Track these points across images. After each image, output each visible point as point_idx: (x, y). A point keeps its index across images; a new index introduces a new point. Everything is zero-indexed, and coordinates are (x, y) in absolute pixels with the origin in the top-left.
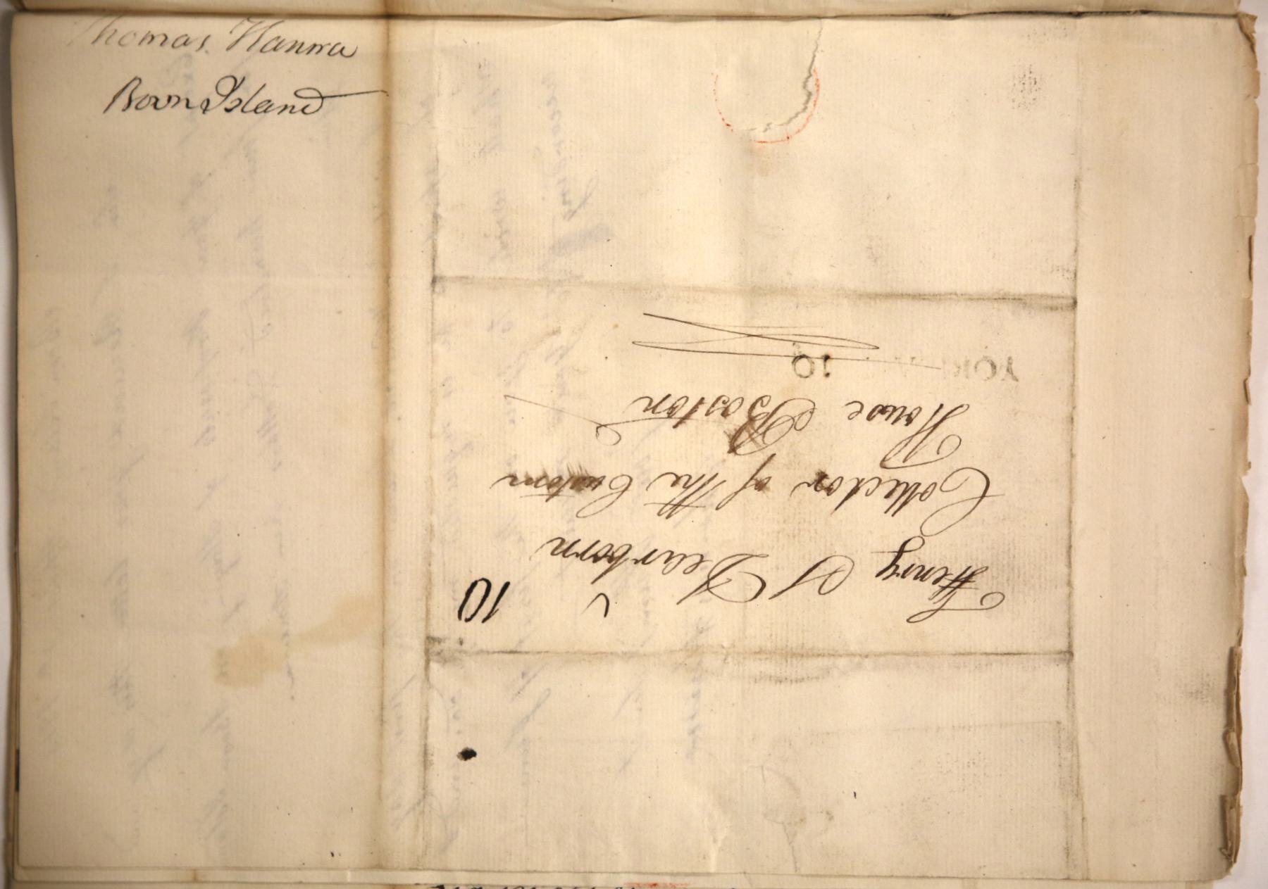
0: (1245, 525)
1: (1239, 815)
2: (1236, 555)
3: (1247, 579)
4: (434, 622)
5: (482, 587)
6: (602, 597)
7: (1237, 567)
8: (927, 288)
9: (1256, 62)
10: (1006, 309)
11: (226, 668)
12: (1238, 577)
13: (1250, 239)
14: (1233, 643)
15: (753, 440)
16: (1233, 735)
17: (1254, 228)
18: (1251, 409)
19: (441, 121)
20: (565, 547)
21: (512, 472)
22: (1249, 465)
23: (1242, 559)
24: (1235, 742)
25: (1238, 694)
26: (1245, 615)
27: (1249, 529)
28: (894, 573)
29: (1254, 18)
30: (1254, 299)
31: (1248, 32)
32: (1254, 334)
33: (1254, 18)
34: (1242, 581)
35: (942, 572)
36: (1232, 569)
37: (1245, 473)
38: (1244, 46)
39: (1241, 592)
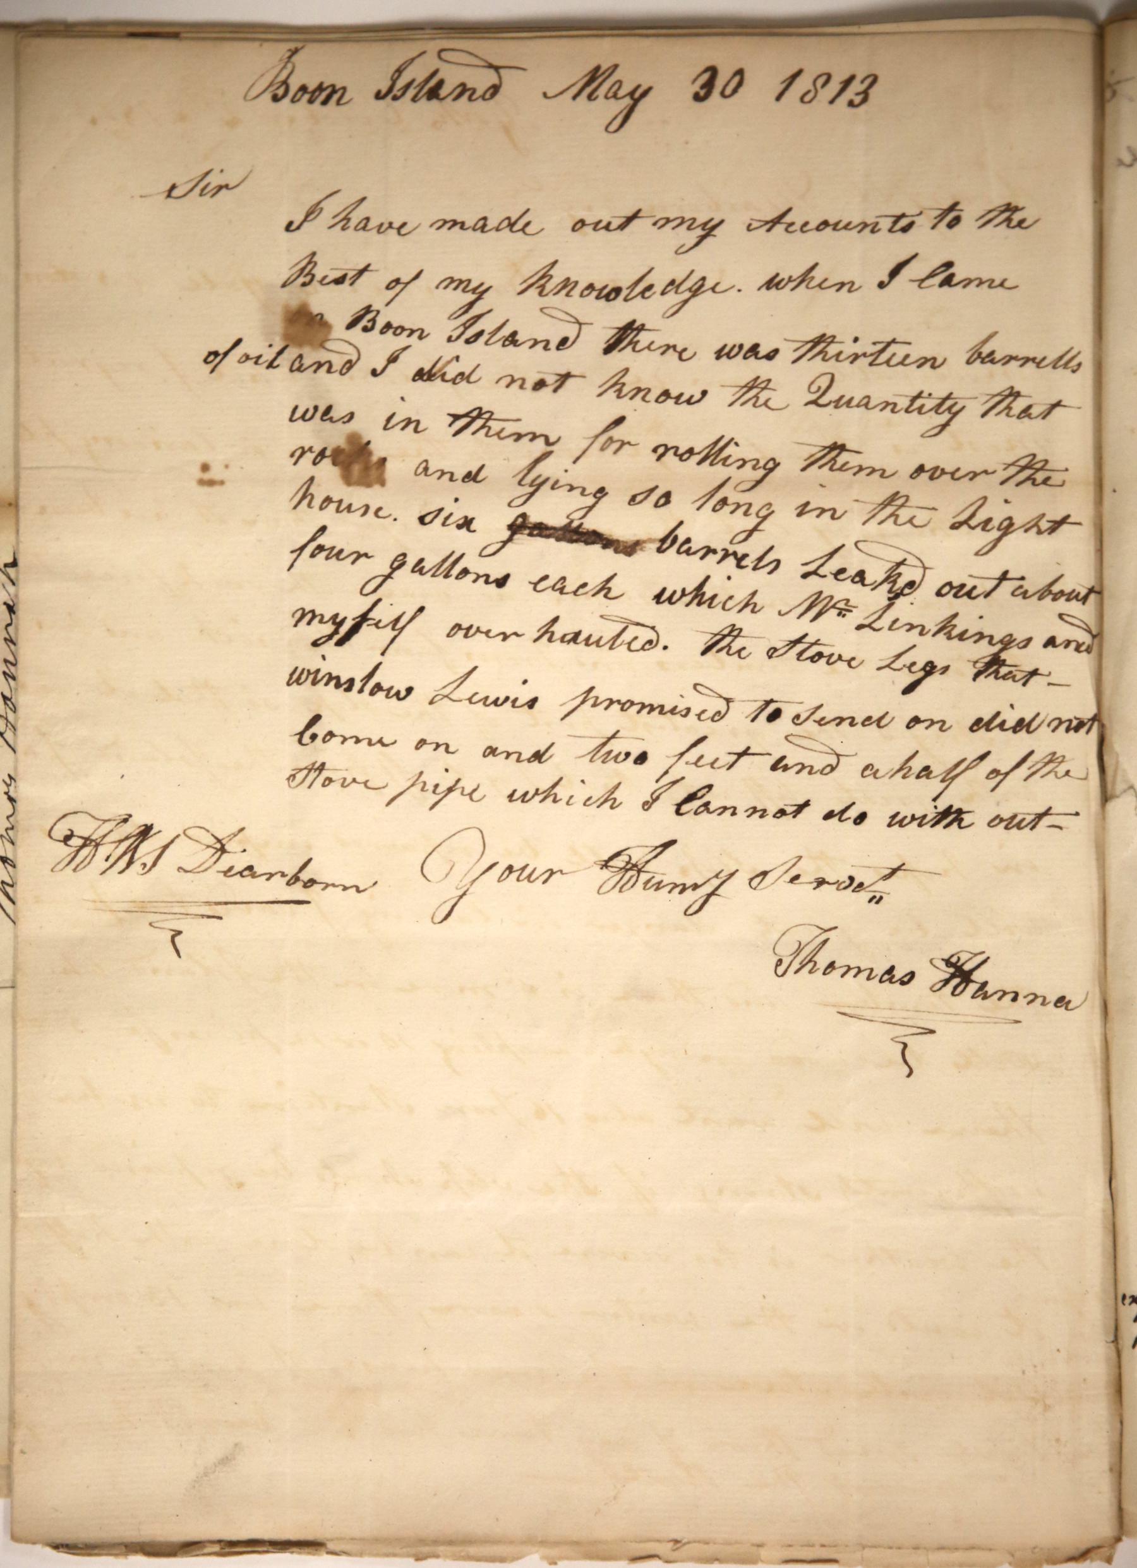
1: (116, 1555)
2: (441, 1549)
3: (411, 1560)
5: (728, 91)
7: (425, 1549)
9: (1054, 1563)
12: (413, 1551)
13: (835, 1561)
14: (331, 1546)
15: (219, 841)
16: (216, 1548)
19: (1009, 1218)
20: (336, 97)
23: (437, 1556)
25: (267, 1552)
28: (1028, 479)
29: (1109, 1560)
31: (1092, 1554)
33: (1109, 1560)
34: (408, 1556)
35: (684, 808)
36: (422, 1541)
37: (543, 1558)
38: (1077, 1554)
39: (395, 1555)
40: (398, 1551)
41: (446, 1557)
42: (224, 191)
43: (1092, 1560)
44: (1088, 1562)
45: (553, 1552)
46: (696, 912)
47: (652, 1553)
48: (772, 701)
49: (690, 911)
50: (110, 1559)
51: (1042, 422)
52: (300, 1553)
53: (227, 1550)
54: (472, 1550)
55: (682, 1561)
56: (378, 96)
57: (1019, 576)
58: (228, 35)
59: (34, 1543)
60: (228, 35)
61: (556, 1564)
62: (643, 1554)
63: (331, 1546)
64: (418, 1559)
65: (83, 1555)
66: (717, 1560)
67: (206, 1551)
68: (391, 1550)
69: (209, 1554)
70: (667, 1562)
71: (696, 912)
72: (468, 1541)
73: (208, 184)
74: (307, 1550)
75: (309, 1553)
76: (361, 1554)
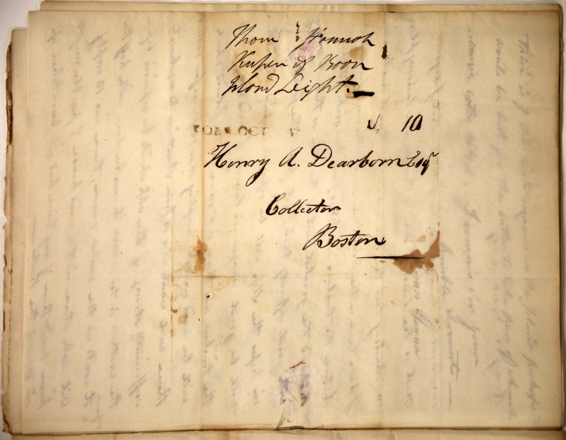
0: (5, 200)
1: (7, 68)
3: (5, 176)
13: (4, 330)
17: (3, 335)
23: (6, 185)
26: (5, 159)
27: (4, 198)
29: (4, 431)
31: (6, 424)
32: (2, 287)
33: (4, 431)
34: (6, 174)
36: (12, 179)
37: (5, 223)
39: (7, 170)
40: (8, 171)
41: (6, 188)
45: (8, 227)
54: (8, 198)
62: (7, 261)
63: (10, 146)
66: (5, 287)
69: (7, 102)
70: (4, 269)
76: (7, 157)
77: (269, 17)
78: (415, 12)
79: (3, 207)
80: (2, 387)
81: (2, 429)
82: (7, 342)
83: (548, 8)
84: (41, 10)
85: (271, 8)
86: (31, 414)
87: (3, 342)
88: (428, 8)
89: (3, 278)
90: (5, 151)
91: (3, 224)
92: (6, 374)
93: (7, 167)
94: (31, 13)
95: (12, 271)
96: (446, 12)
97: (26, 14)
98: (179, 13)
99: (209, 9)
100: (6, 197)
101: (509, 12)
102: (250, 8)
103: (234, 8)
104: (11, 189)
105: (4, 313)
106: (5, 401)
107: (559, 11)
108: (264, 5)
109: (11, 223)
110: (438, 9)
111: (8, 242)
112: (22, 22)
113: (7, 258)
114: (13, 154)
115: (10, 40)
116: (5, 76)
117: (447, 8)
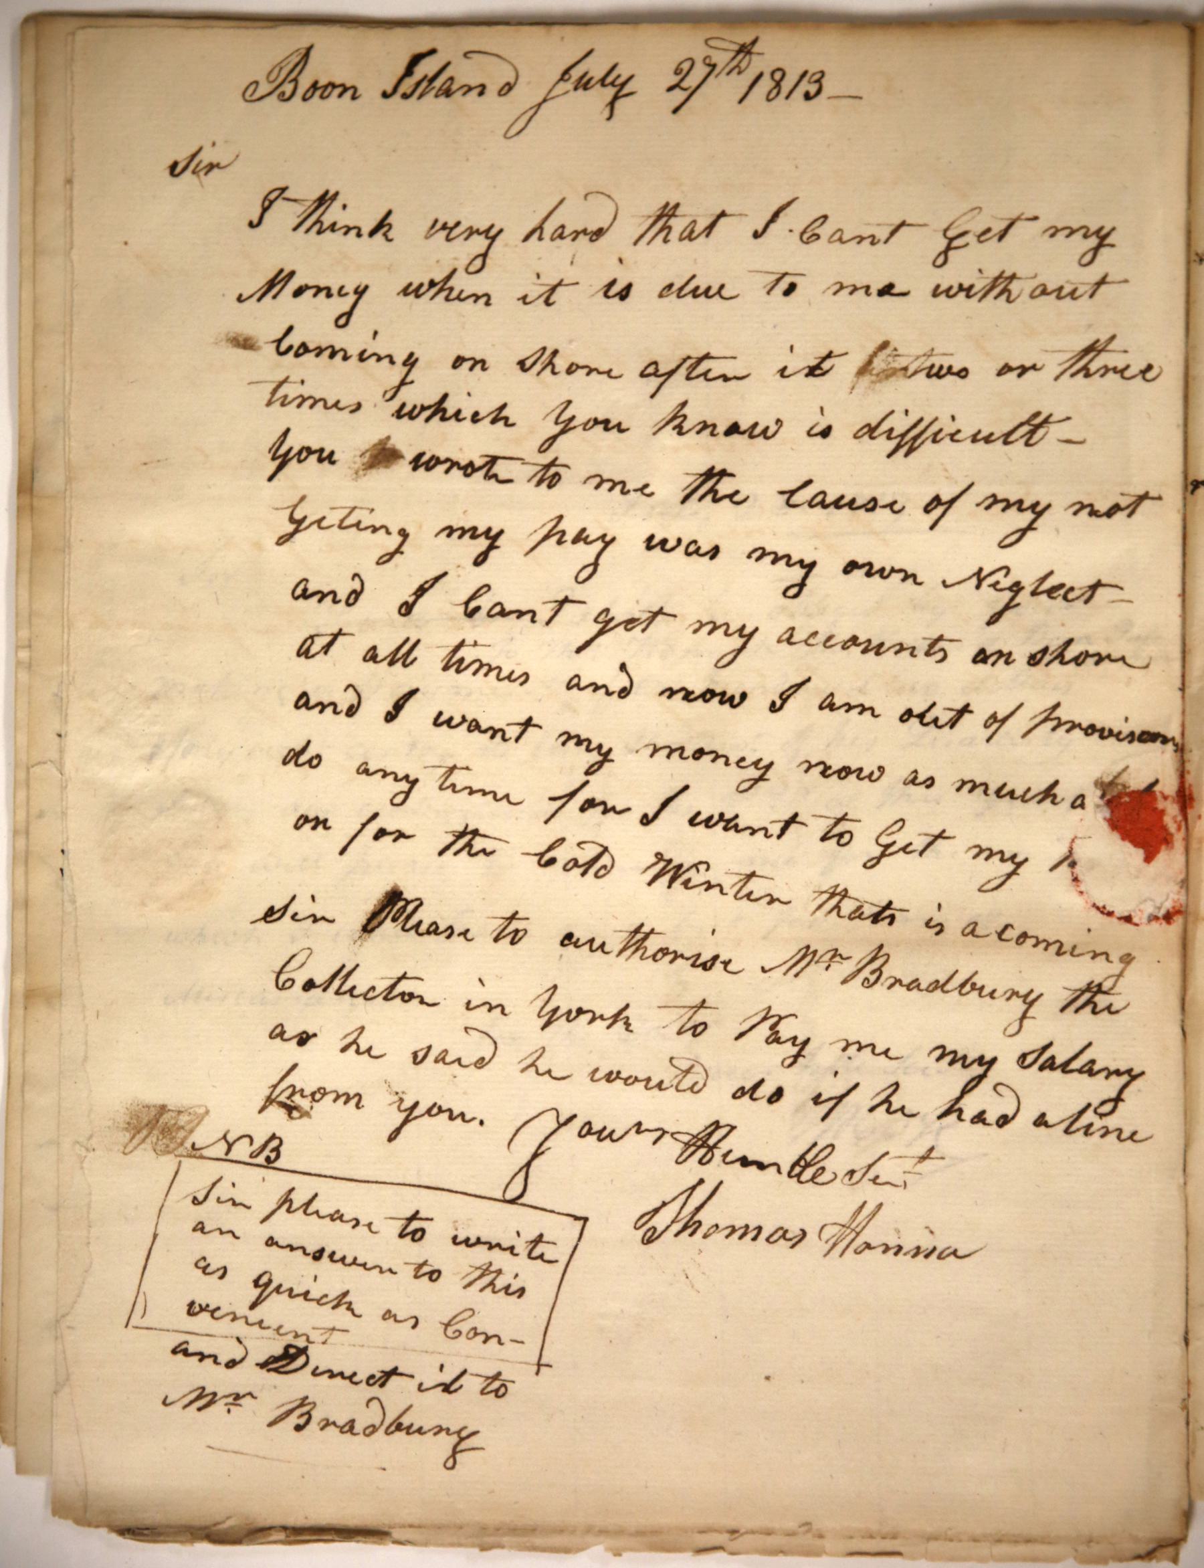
0: (544, 1550)
1: (182, 1542)
3: (476, 1550)
4: (528, 1360)
6: (351, 689)
7: (490, 1540)
8: (851, 100)
10: (799, 680)
11: (69, 1327)
13: (899, 1554)
17: (913, 1557)
18: (688, 1555)
21: (1012, 305)
22: (618, 1554)
23: (502, 1547)
24: (272, 1538)
25: (333, 1541)
26: (432, 1548)
27: (538, 1554)
29: (1175, 1560)
30: (825, 1559)
31: (1157, 1554)
32: (781, 1559)
33: (1175, 1560)
34: (473, 1546)
36: (483, 1529)
37: (607, 1549)
39: (460, 1545)
40: (463, 1541)
41: (511, 1547)
42: (216, 170)
43: (1158, 1560)
44: (1154, 1562)
45: (619, 1542)
46: (724, 666)
47: (717, 1544)
48: (785, 274)
49: (720, 664)
50: (177, 1546)
51: (1090, 302)
52: (365, 1542)
53: (292, 1538)
54: (538, 1541)
55: (747, 1552)
56: (385, 95)
57: (1064, 417)
58: (308, 1538)
59: (97, 1526)
60: (308, 1538)
61: (620, 1555)
62: (709, 1545)
63: (396, 1534)
64: (484, 1548)
65: (149, 1541)
66: (782, 1552)
67: (272, 1538)
68: (455, 1540)
69: (275, 1542)
70: (732, 1554)
71: (724, 666)
72: (533, 1530)
73: (201, 162)
74: (372, 1539)
75: (375, 1543)
76: (426, 1544)
77: (41, 815)
78: (34, 412)
79: (563, 1555)
80: (1055, 1560)
81: (1171, 1565)
82: (933, 1546)
83: (30, 57)
84: (15, 1444)
85: (21, 815)
86: (1111, 1468)
87: (931, 1557)
88: (27, 381)
89: (757, 1558)
90: (408, 1550)
91: (610, 1554)
92: (1022, 1549)
93: (452, 1545)
94: (20, 1469)
95: (733, 1532)
96: (36, 327)
97: (23, 1480)
98: (27, 1060)
99: (19, 984)
100: (534, 1548)
101: (37, 158)
102: (20, 870)
103: (20, 915)
104: (514, 1530)
105: (851, 1554)
106: (1087, 1545)
107: (37, 21)
108: (15, 833)
109: (603, 1532)
110: (27, 355)
111: (658, 1540)
112: (35, 1489)
113: (701, 1545)
114: (411, 1526)
115: (103, 1531)
116: (204, 1547)
117: (27, 330)
